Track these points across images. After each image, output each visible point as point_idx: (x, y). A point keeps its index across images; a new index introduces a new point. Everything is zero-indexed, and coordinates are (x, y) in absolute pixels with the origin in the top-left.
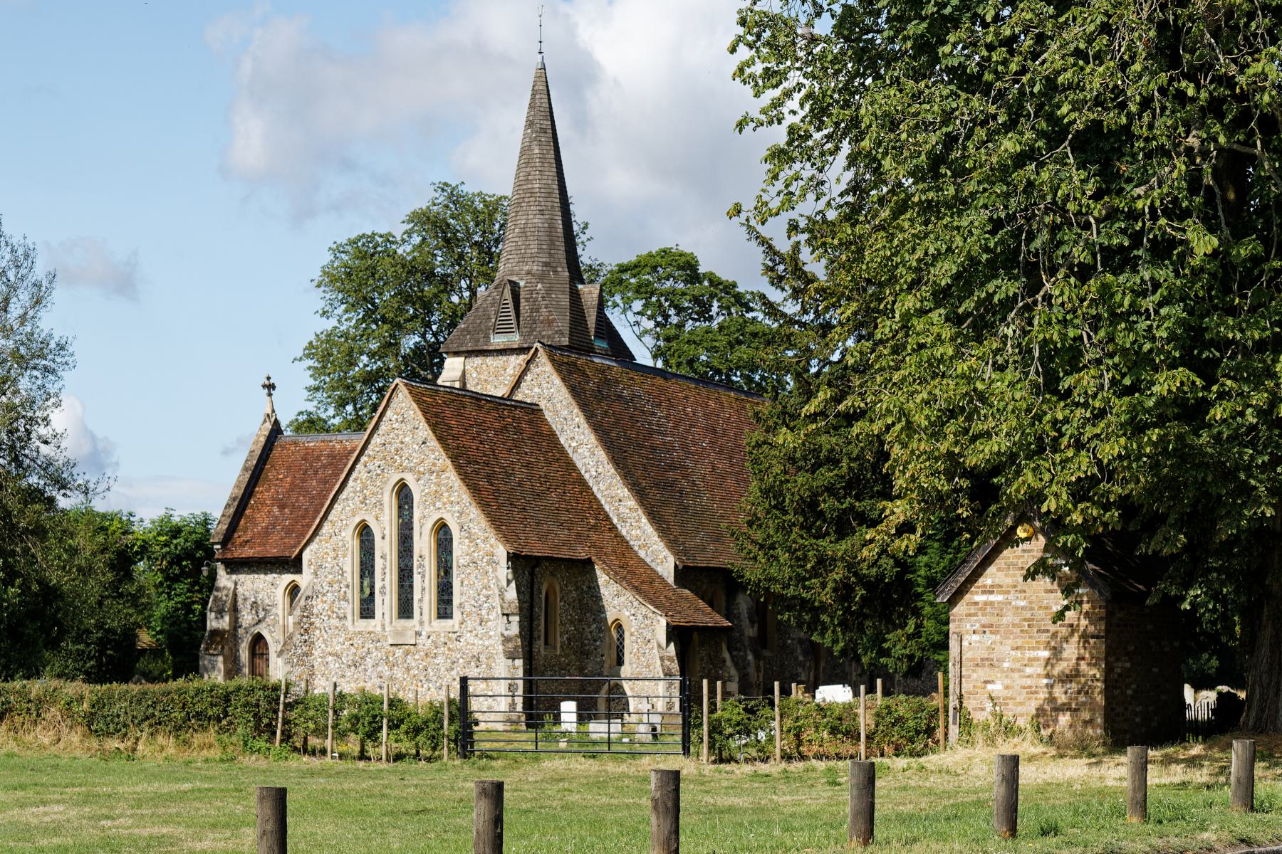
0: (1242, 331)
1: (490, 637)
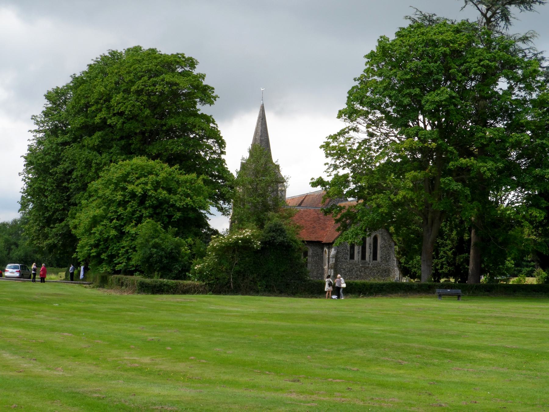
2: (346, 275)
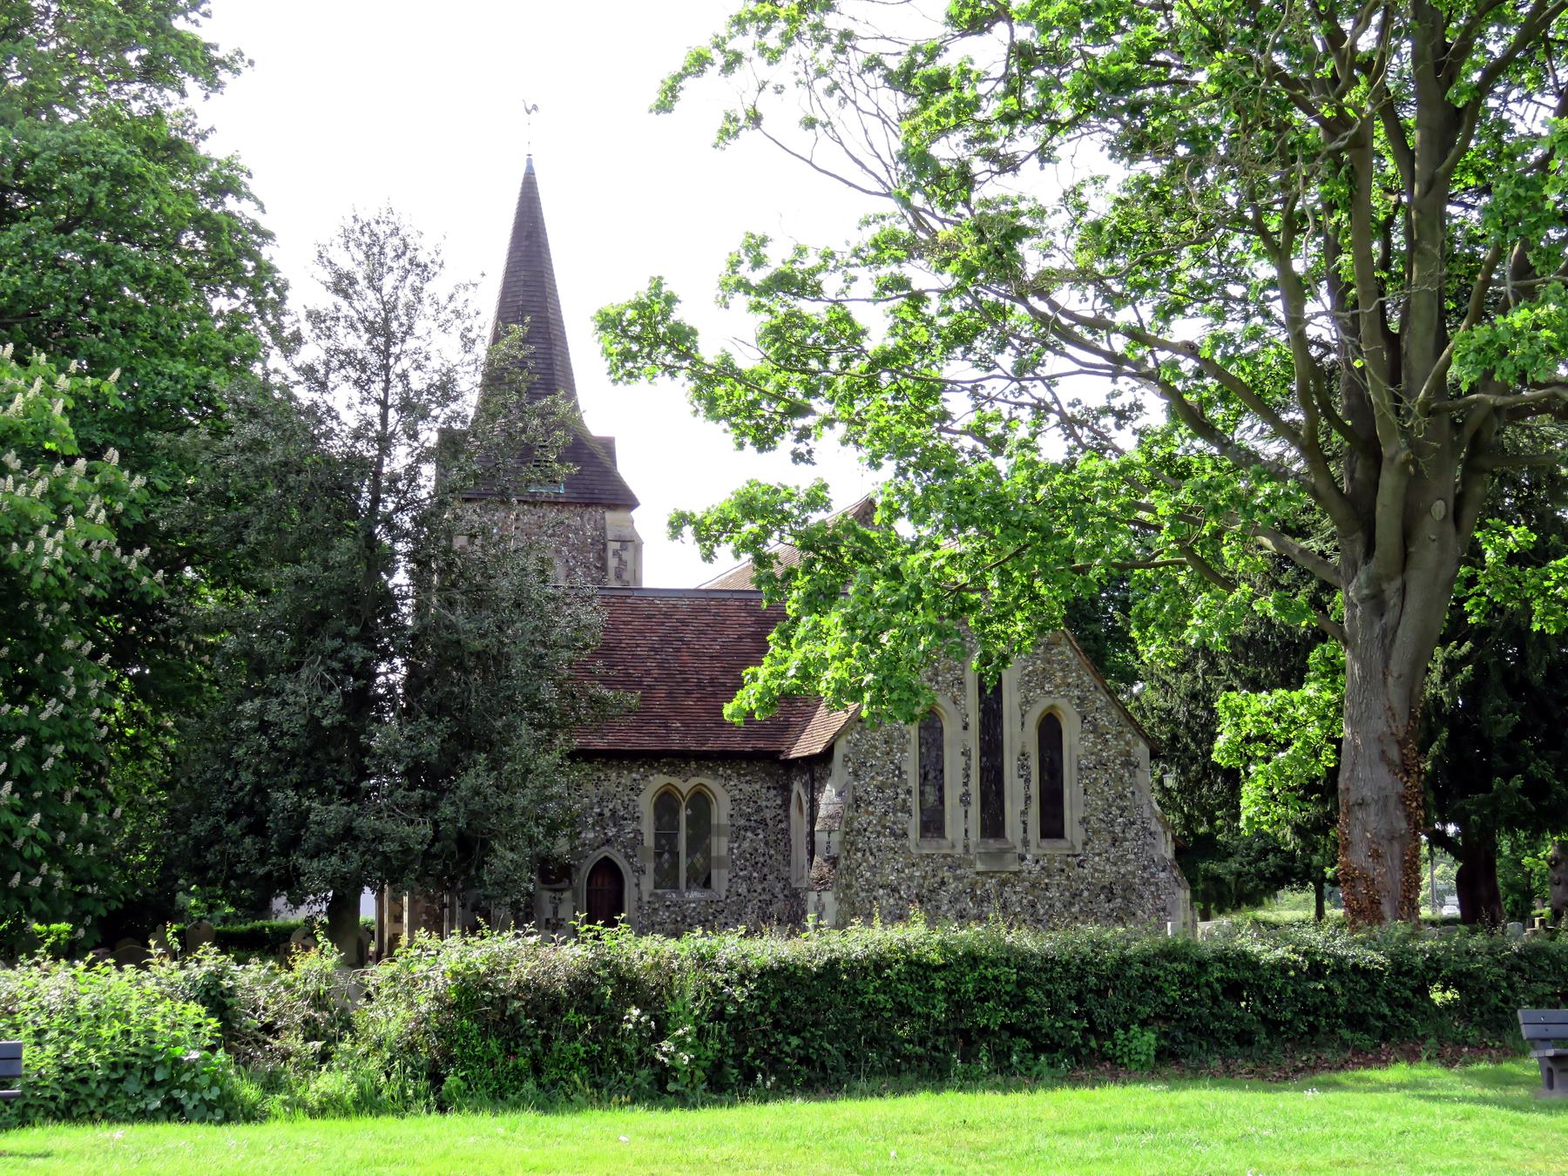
0: (36, 528)
1: (1128, 862)
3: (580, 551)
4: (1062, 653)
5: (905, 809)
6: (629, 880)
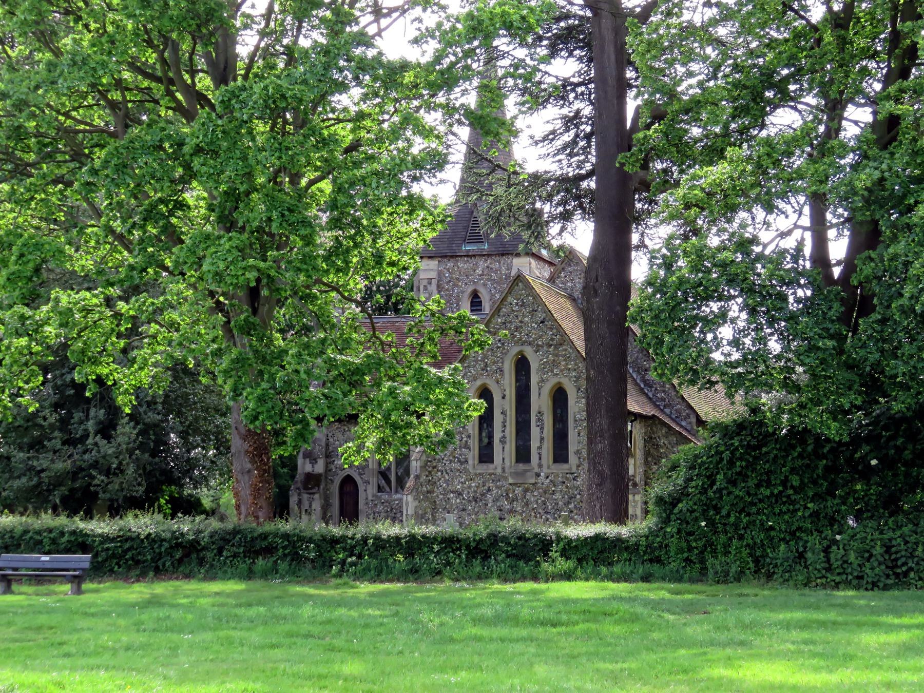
2: (464, 510)
3: (498, 283)
4: (566, 350)
5: (467, 446)
6: (361, 488)
